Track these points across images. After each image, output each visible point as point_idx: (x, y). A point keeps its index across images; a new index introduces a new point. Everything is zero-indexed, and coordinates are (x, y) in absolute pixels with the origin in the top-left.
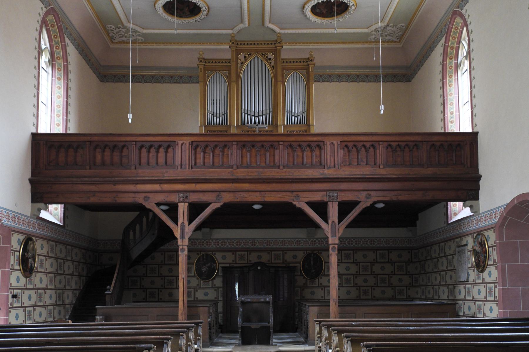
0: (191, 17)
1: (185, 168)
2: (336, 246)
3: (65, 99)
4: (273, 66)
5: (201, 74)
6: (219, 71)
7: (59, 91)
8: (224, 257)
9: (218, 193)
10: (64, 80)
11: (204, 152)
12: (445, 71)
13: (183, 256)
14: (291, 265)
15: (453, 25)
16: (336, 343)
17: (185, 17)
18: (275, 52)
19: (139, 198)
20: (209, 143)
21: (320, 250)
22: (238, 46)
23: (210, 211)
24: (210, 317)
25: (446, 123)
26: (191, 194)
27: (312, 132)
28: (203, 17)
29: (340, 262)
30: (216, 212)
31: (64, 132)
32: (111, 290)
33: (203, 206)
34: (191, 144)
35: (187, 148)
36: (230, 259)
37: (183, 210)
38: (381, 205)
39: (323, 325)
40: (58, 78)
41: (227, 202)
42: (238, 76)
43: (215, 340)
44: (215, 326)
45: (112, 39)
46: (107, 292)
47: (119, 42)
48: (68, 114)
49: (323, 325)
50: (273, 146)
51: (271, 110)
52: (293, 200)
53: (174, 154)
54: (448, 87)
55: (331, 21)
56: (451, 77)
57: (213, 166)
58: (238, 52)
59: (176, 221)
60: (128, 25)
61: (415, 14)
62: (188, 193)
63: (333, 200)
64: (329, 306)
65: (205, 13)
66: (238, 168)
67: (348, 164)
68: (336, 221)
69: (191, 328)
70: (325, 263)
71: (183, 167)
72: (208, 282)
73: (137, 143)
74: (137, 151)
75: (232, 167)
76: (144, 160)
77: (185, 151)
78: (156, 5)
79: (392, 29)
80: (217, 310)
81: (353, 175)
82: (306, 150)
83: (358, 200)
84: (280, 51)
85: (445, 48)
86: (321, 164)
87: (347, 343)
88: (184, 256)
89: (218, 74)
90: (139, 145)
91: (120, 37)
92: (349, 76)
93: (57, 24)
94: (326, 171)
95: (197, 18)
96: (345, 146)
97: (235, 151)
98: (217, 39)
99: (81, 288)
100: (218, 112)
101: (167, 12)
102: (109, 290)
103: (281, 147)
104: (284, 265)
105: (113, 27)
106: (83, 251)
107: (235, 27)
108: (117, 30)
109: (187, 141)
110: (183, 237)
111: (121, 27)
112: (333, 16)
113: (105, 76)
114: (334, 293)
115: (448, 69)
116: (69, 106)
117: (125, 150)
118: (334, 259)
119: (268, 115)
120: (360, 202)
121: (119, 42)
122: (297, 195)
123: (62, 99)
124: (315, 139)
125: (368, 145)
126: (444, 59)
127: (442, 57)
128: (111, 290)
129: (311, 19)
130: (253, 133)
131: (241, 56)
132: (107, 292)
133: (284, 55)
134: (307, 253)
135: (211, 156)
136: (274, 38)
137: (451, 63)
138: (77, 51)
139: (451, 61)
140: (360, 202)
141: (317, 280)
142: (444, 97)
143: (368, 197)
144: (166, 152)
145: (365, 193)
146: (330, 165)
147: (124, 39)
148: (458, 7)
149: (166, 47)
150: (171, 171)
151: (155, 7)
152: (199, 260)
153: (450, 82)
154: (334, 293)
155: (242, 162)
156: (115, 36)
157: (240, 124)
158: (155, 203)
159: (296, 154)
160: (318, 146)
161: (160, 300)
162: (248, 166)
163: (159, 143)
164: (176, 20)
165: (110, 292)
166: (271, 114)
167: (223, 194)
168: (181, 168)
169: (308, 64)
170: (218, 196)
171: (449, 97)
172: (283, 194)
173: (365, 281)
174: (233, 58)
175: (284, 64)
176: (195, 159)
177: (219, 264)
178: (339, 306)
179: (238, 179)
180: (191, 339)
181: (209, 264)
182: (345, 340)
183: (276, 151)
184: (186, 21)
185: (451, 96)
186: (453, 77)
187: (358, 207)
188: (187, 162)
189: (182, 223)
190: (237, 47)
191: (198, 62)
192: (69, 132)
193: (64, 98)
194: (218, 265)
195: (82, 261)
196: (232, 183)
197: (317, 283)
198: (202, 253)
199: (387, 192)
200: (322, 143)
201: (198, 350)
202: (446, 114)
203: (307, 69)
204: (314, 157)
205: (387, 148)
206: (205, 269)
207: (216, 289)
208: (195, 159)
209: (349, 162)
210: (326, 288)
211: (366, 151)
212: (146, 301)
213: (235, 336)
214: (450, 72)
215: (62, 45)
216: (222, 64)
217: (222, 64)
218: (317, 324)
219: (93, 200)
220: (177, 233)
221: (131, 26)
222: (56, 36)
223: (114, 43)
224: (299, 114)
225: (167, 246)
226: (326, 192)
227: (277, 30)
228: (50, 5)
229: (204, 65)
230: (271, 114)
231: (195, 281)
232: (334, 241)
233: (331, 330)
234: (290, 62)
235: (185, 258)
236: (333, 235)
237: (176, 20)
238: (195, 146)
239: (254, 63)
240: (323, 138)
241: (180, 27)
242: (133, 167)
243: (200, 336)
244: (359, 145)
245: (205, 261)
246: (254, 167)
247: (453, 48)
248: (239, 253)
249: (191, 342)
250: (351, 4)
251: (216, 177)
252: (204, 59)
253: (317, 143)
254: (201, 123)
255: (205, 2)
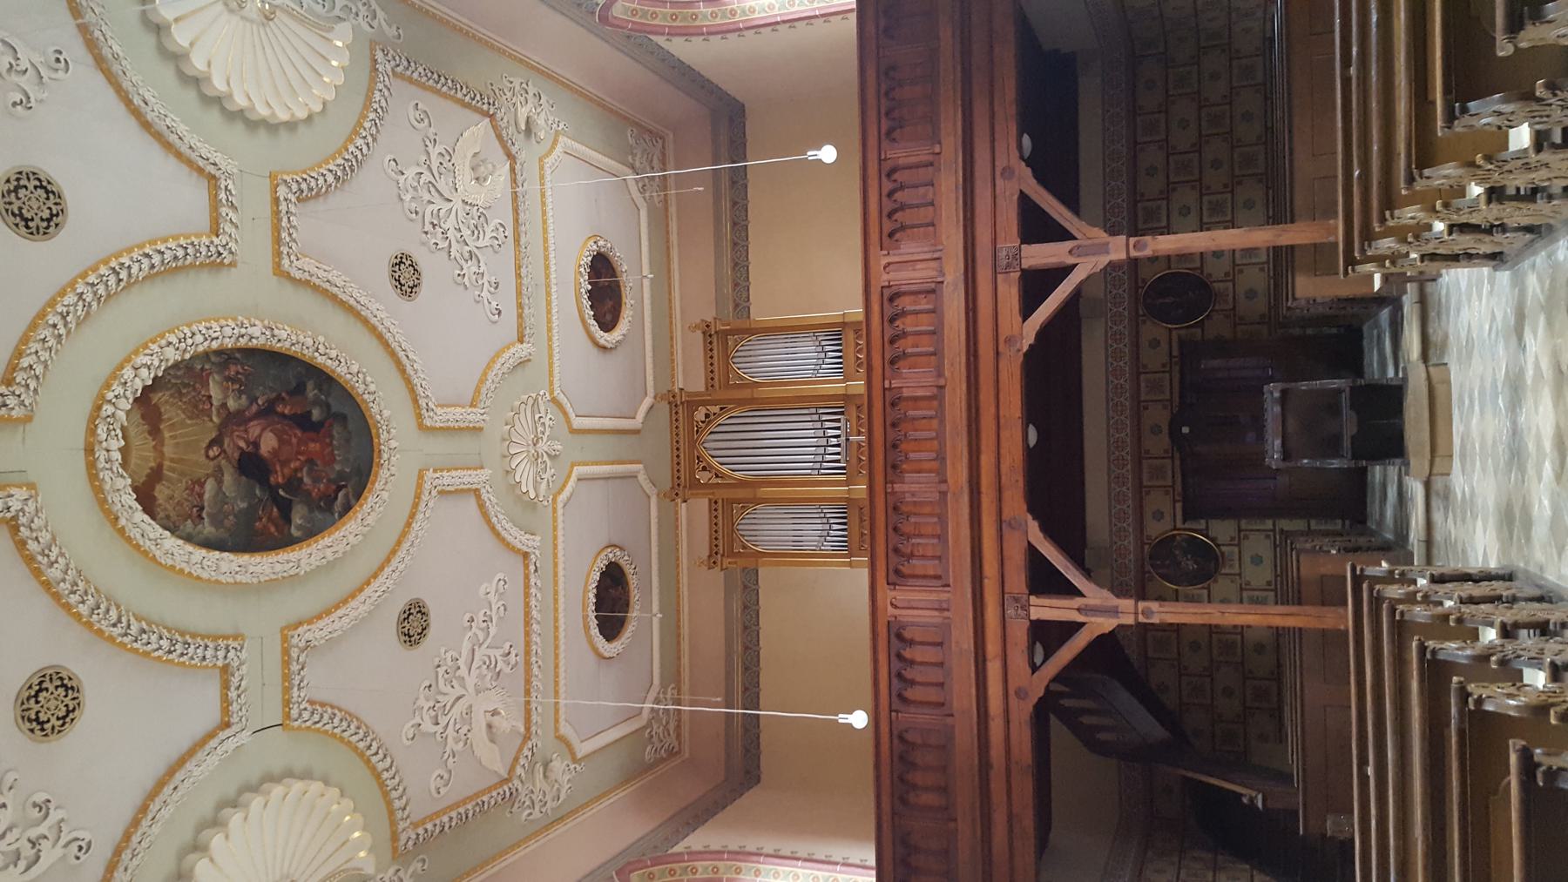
0: (627, 584)
1: (948, 601)
2: (1132, 240)
3: (800, 863)
4: (721, 409)
5: (742, 562)
6: (733, 525)
7: (782, 875)
8: (1158, 515)
9: (1004, 526)
10: (759, 862)
11: (912, 556)
12: (719, 29)
13: (1161, 613)
14: (1175, 353)
15: (628, 21)
16: (1422, 210)
17: (628, 596)
18: (692, 404)
19: (1023, 711)
20: (890, 546)
21: (1136, 282)
22: (682, 484)
23: (1047, 544)
24: (1325, 548)
25: (833, 10)
26: (1007, 590)
27: (861, 318)
28: (626, 558)
29: (1168, 230)
30: (1048, 530)
31: (874, 872)
32: (1254, 794)
33: (1035, 559)
34: (892, 587)
35: (901, 595)
36: (1159, 501)
37: (1047, 609)
38: (1026, 140)
39: (1363, 251)
40: (757, 876)
41: (1025, 507)
42: (742, 484)
43: (1389, 536)
44: (1348, 538)
45: (672, 753)
46: (1260, 805)
47: (678, 736)
48: (832, 859)
49: (1363, 251)
50: (894, 401)
51: (814, 411)
52: (1019, 350)
53: (917, 625)
54: (756, 15)
55: (628, 289)
56: (733, 13)
57: (942, 537)
58: (695, 484)
59: (1075, 627)
60: (646, 715)
61: (611, 111)
62: (1006, 596)
63: (1018, 256)
64: (1292, 247)
65: (618, 553)
66: (945, 481)
67: (931, 228)
68: (1069, 244)
69: (1375, 592)
70: (1169, 268)
71: (945, 606)
72: (1223, 554)
73: (894, 708)
74: (912, 709)
75: (944, 494)
76: (932, 695)
77: (909, 601)
78: (607, 655)
79: (639, 156)
80: (1302, 533)
81: (957, 216)
82: (901, 327)
83: (1015, 197)
84: (690, 394)
85: (673, 33)
86: (933, 291)
87: (1428, 178)
88: (1162, 609)
89: (740, 527)
90: (897, 704)
91: (669, 735)
92: (735, 244)
93: (647, 867)
94: (949, 279)
95: (628, 570)
96: (892, 237)
97: (906, 487)
98: (670, 527)
99: (1248, 867)
100: (820, 527)
101: (619, 632)
102: (1252, 800)
103: (895, 384)
104: (1177, 368)
105: (649, 748)
106: (1150, 853)
107: (645, 492)
108: (655, 739)
109: (887, 594)
110: (1115, 612)
111: (648, 731)
112: (617, 284)
113: (748, 772)
114: (1261, 237)
115: (718, 21)
116: (814, 857)
117: (910, 737)
118: (1165, 244)
119: (825, 417)
120: (1021, 191)
121: (678, 736)
122: (1005, 342)
123: (800, 871)
124: (876, 308)
125: (888, 186)
126: (697, 32)
127: (694, 39)
128: (1254, 794)
129: (624, 332)
130: (865, 449)
131: (703, 477)
132: (1260, 805)
133: (698, 385)
134: (1143, 316)
135: (919, 541)
136: (664, 408)
137: (705, 16)
138: (709, 822)
139: (700, 17)
140: (1021, 191)
141: (1216, 285)
142: (777, 23)
143: (1008, 172)
144: (911, 643)
145: (1000, 182)
146: (933, 269)
147: (672, 726)
148: (593, 13)
149: (686, 638)
150: (955, 633)
151: (610, 658)
152: (1165, 577)
153: (744, 12)
154: (1261, 237)
155: (930, 471)
156: (667, 745)
157: (843, 478)
158: (1033, 673)
159: (910, 350)
160: (891, 300)
161: (1277, 675)
162: (940, 457)
163: (893, 658)
164: (634, 615)
165: (1260, 797)
166: (821, 411)
167: (1006, 516)
168: (948, 610)
169: (716, 332)
170: (1010, 524)
171: (776, 12)
172: (1004, 376)
173: (1216, 164)
174: (707, 494)
175: (717, 385)
176: (925, 577)
177: (1175, 529)
178: (1292, 222)
179: (970, 482)
180: (1408, 594)
181: (1177, 552)
182: (1419, 185)
183: (905, 395)
184: (635, 595)
185: (774, 8)
186: (735, 7)
187: (1034, 197)
188: (933, 597)
189: (1080, 613)
190: (685, 487)
191: (717, 569)
192: (872, 861)
193: (796, 867)
194: (1179, 529)
195: (1176, 859)
196: (979, 493)
197: (1221, 285)
198: (1146, 569)
199: (997, 128)
200: (885, 290)
201: (1432, 576)
202: (812, 14)
203: (726, 333)
204: (918, 308)
205: (894, 139)
206: (1189, 562)
207: (1239, 539)
208: (925, 577)
209: (928, 225)
210: (1237, 260)
211: (902, 188)
212: (1280, 709)
213: (1373, 487)
214: (724, 16)
215: (688, 861)
216: (720, 518)
217: (720, 518)
218: (1353, 270)
219: (1028, 821)
220: (1106, 624)
221: (648, 705)
222: (671, 870)
223: (680, 749)
224: (820, 349)
225: (1132, 652)
226: (999, 276)
227: (648, 401)
228: (612, 877)
229: (723, 555)
230: (821, 411)
231: (1222, 585)
232: (1118, 249)
233: (1383, 229)
234: (712, 372)
235: (1169, 607)
236: (1103, 249)
237: (634, 613)
238: (897, 577)
239: (715, 449)
240: (873, 289)
241: (647, 607)
242: (949, 720)
243: (1391, 572)
244: (888, 206)
245: (1167, 562)
246: (942, 445)
247: (674, 14)
248: (1145, 476)
249: (1415, 593)
250: (595, 247)
251: (965, 532)
252: (710, 556)
253: (886, 302)
254: (843, 564)
255: (599, 554)
